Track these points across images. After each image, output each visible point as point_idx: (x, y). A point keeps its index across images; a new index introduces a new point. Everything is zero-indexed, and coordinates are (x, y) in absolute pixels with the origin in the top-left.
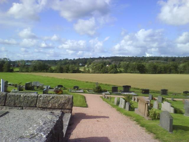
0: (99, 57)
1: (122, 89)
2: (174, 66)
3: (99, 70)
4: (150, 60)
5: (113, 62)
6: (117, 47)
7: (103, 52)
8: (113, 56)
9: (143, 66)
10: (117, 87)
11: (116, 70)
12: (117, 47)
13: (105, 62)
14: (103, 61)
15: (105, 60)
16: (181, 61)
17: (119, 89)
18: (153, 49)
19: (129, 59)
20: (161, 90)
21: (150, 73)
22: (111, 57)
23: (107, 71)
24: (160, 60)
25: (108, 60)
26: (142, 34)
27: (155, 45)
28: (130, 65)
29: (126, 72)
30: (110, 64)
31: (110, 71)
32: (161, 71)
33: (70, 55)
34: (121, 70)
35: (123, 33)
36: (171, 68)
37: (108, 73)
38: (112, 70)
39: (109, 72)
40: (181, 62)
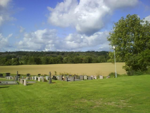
0: (5, 51)
1: (6, 75)
2: (60, 59)
3: (4, 63)
4: (47, 54)
5: (18, 56)
6: (21, 43)
7: (8, 46)
8: (18, 50)
9: (39, 59)
10: (3, 74)
11: (18, 62)
12: (21, 43)
13: (11, 56)
14: (9, 55)
15: (10, 55)
16: (67, 54)
17: (4, 75)
18: (50, 45)
19: (31, 54)
20: (27, 74)
21: (44, 63)
22: (16, 52)
23: (10, 63)
24: (54, 54)
25: (13, 54)
26: (39, 34)
27: (50, 42)
28: (29, 59)
29: (26, 64)
30: (15, 57)
31: (13, 63)
32: (52, 62)
33: (78, 28)
34: (22, 62)
35: (21, 31)
36: (59, 60)
37: (11, 65)
38: (15, 63)
39: (12, 64)
40: (67, 55)
